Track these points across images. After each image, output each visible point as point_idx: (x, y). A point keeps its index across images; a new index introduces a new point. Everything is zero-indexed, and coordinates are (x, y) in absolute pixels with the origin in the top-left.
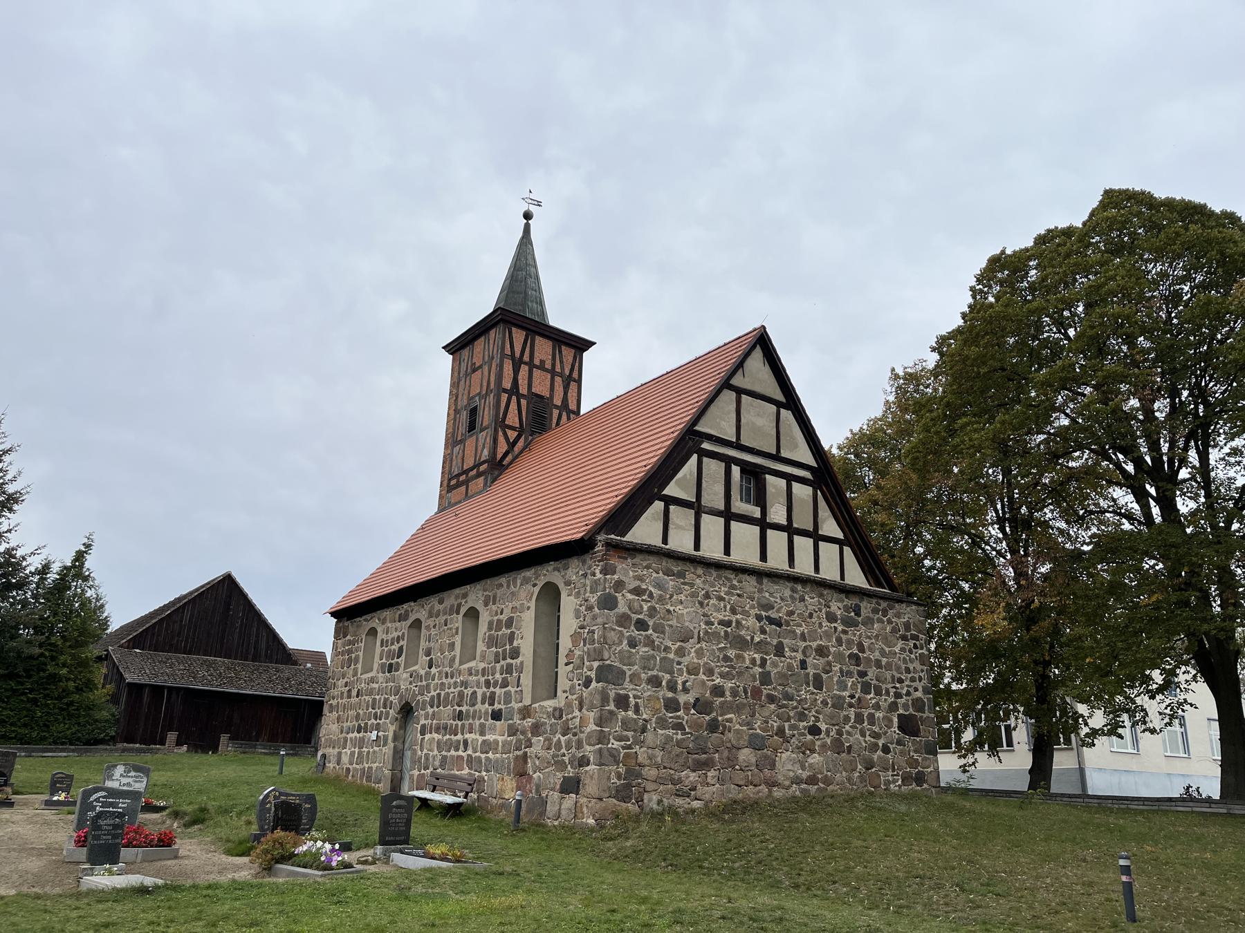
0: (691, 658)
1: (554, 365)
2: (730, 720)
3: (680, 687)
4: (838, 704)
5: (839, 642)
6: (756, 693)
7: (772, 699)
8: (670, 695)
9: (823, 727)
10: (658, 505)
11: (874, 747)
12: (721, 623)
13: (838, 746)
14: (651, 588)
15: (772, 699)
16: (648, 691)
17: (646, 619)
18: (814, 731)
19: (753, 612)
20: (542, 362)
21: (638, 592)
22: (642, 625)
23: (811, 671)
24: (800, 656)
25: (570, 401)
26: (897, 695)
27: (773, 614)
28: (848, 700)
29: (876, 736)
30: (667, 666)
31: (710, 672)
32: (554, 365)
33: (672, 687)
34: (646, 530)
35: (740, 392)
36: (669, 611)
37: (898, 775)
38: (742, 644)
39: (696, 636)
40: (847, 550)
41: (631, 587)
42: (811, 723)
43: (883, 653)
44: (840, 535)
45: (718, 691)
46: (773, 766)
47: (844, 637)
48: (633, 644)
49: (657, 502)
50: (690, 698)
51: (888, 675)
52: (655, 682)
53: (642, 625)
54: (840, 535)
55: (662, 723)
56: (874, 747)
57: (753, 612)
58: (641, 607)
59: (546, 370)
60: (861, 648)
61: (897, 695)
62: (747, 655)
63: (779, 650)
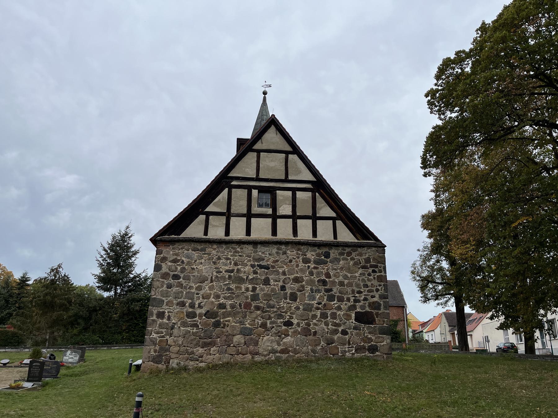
0: (206, 290)
2: (229, 321)
3: (197, 306)
4: (309, 308)
5: (311, 274)
6: (247, 306)
7: (258, 308)
8: (190, 310)
9: (295, 321)
10: (202, 217)
11: (335, 332)
12: (227, 271)
13: (306, 332)
14: (184, 259)
15: (258, 308)
16: (178, 309)
17: (179, 274)
18: (289, 324)
19: (249, 263)
21: (175, 261)
22: (176, 277)
23: (289, 291)
24: (281, 284)
26: (356, 301)
27: (263, 263)
28: (315, 305)
29: (338, 325)
30: (190, 296)
31: (217, 297)
33: (192, 306)
35: (259, 152)
36: (193, 269)
37: (352, 347)
38: (241, 280)
39: (209, 280)
40: (339, 223)
41: (171, 259)
42: (286, 320)
43: (346, 277)
44: (333, 215)
45: (222, 306)
46: (256, 343)
48: (169, 286)
49: (201, 216)
50: (203, 311)
51: (349, 290)
52: (183, 304)
53: (176, 277)
54: (333, 215)
55: (184, 324)
57: (249, 263)
58: (177, 268)
60: (328, 275)
61: (356, 301)
62: (243, 287)
63: (266, 282)
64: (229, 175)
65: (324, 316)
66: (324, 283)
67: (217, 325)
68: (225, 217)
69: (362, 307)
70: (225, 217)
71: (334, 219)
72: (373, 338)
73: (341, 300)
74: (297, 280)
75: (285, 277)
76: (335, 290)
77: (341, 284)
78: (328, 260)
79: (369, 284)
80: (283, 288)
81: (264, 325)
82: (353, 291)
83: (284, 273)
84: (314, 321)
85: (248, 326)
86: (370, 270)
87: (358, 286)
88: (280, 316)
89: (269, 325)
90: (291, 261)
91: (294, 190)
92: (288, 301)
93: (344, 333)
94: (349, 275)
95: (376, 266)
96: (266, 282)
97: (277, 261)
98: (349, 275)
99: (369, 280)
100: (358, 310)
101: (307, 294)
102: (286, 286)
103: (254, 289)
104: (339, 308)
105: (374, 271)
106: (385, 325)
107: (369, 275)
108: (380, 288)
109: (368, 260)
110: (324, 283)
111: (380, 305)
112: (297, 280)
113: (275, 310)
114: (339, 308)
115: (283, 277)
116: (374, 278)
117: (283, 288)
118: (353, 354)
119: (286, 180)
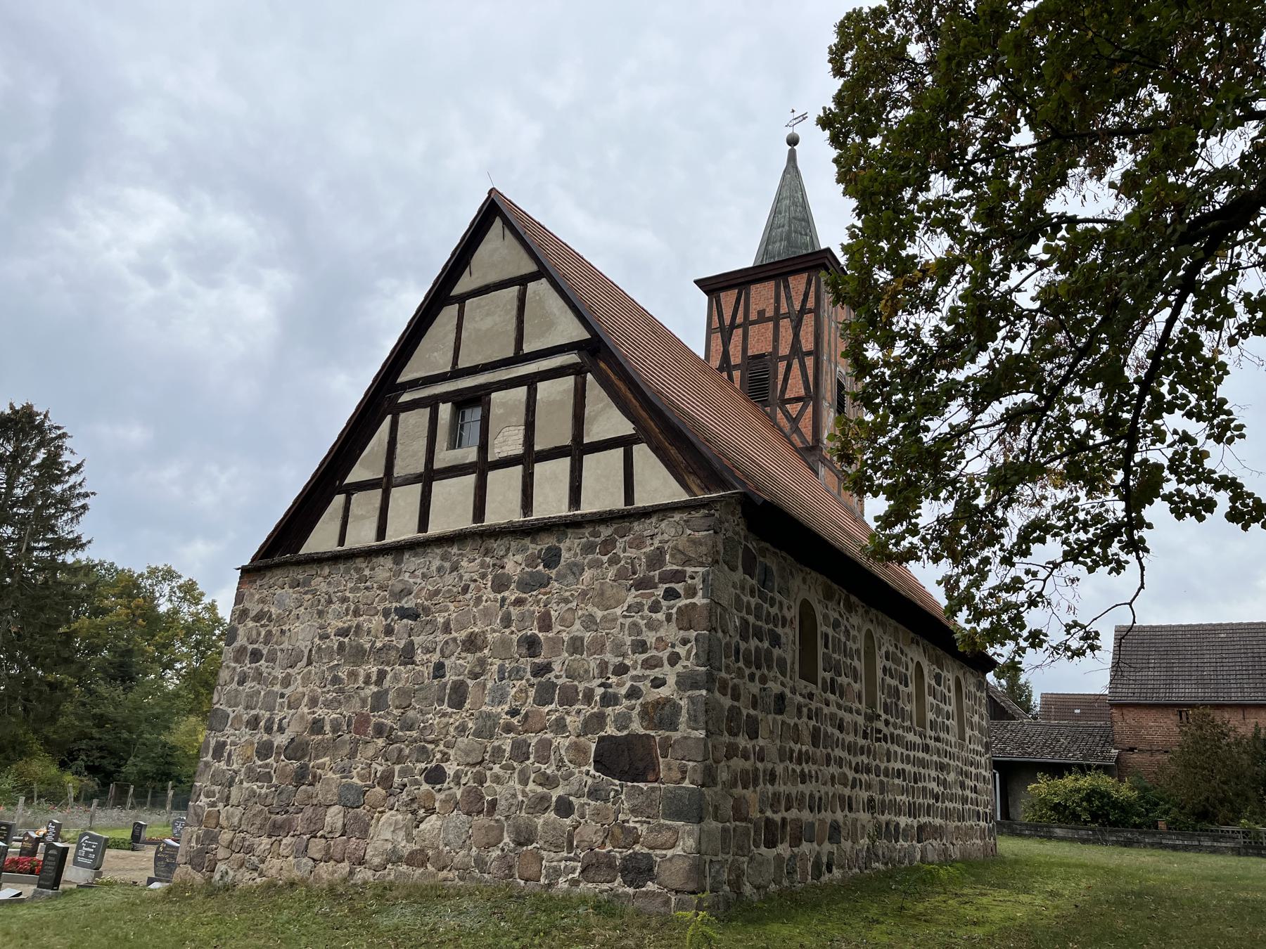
1: (777, 309)
2: (322, 766)
4: (487, 728)
5: (507, 621)
6: (363, 721)
9: (451, 768)
10: (339, 500)
11: (540, 804)
15: (379, 730)
18: (435, 776)
20: (761, 313)
23: (450, 678)
25: (803, 342)
27: (408, 603)
32: (777, 309)
34: (321, 539)
35: (462, 299)
38: (359, 655)
39: (305, 659)
40: (642, 452)
43: (590, 622)
44: (627, 428)
47: (515, 612)
54: (627, 428)
56: (540, 804)
59: (769, 319)
61: (609, 700)
63: (407, 656)
64: (399, 380)
65: (520, 752)
66: (531, 645)
67: (301, 777)
68: (380, 490)
69: (623, 721)
70: (380, 490)
71: (625, 443)
72: (642, 829)
73: (568, 698)
74: (472, 644)
75: (447, 637)
76: (557, 667)
77: (576, 645)
78: (553, 573)
79: (650, 637)
80: (439, 670)
81: (386, 780)
82: (603, 666)
83: (447, 628)
84: (496, 768)
85: (356, 780)
86: (660, 592)
87: (618, 649)
88: (424, 754)
89: (397, 780)
90: (465, 589)
91: (530, 382)
92: (445, 707)
93: (564, 808)
94: (599, 614)
95: (678, 576)
96: (407, 656)
97: (437, 592)
98: (599, 614)
99: (651, 626)
100: (610, 730)
101: (490, 685)
102: (447, 662)
103: (382, 675)
104: (560, 726)
105: (671, 594)
106: (686, 784)
107: (655, 608)
108: (682, 651)
109: (656, 559)
110: (531, 645)
111: (676, 709)
112: (472, 644)
113: (414, 734)
114: (560, 726)
115: (441, 638)
116: (669, 618)
117: (439, 670)
118: (575, 883)
119: (520, 358)
